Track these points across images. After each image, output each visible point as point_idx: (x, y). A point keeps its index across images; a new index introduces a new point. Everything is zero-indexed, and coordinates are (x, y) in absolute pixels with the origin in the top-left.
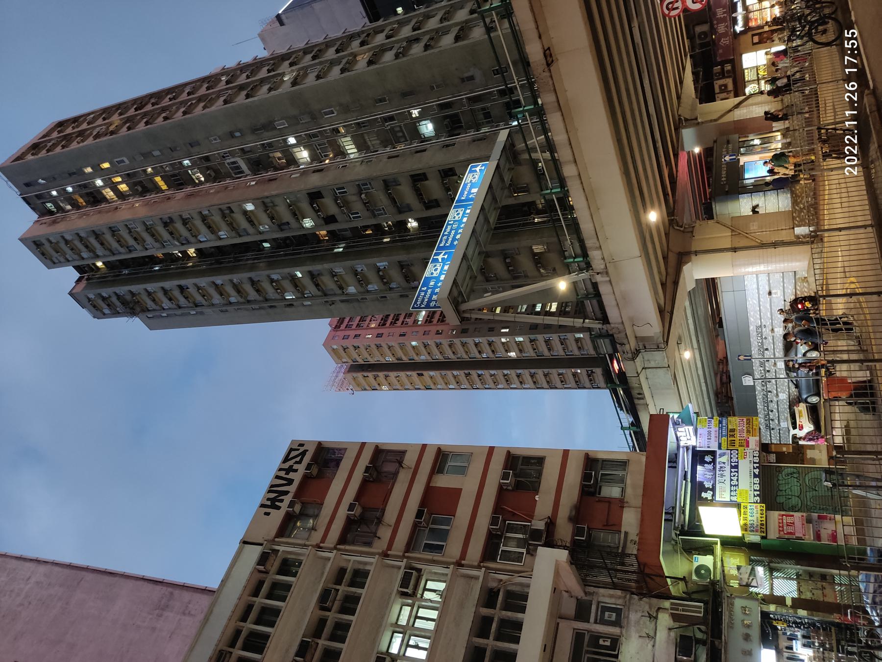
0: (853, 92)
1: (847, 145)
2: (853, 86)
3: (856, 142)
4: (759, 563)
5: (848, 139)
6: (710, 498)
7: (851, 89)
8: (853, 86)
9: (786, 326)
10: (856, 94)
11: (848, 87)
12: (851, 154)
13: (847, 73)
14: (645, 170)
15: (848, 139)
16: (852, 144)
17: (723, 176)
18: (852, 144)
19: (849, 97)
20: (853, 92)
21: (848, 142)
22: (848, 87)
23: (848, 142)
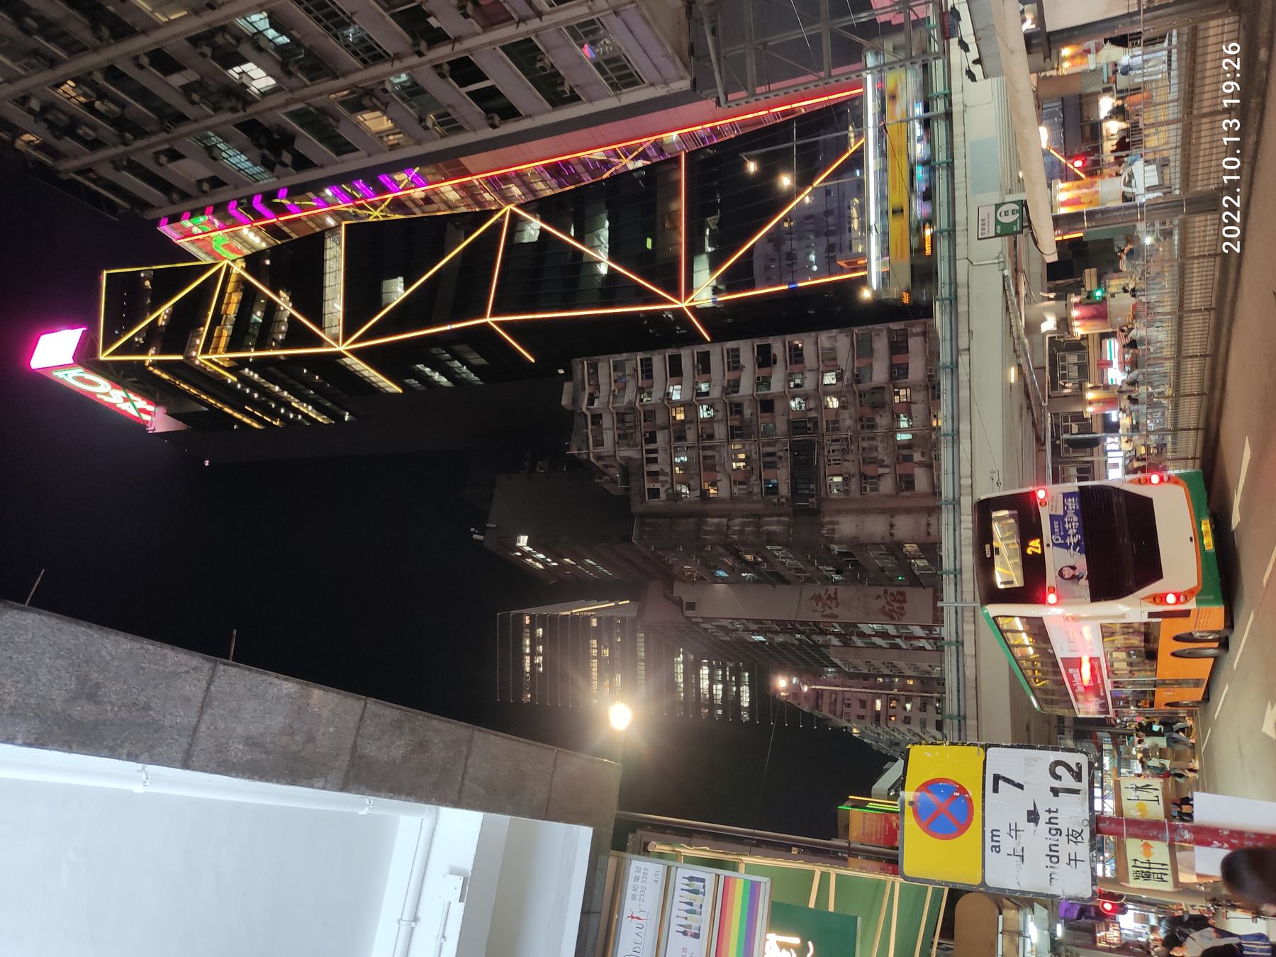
0: (1234, 57)
1: (1226, 225)
2: (1234, 48)
3: (1238, 205)
4: (1059, 53)
5: (1227, 202)
6: (1134, 461)
7: (1231, 52)
8: (1234, 48)
9: (1128, 184)
10: (1238, 59)
11: (1227, 49)
12: (1232, 222)
13: (1226, 182)
14: (879, 803)
15: (1227, 202)
16: (1232, 208)
17: (252, 373)
18: (1232, 208)
19: (1227, 247)
20: (1234, 57)
21: (1226, 68)
22: (1227, 49)
23: (1226, 206)
